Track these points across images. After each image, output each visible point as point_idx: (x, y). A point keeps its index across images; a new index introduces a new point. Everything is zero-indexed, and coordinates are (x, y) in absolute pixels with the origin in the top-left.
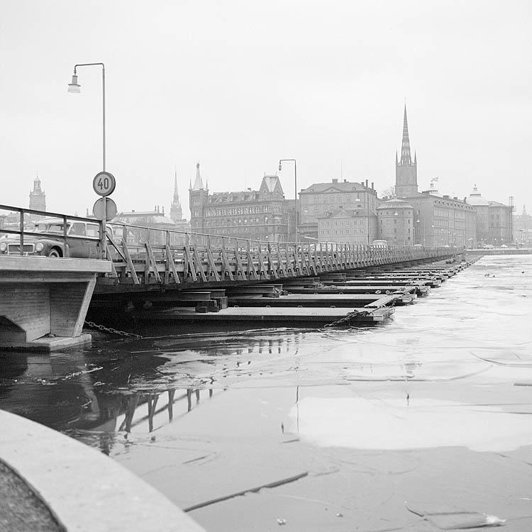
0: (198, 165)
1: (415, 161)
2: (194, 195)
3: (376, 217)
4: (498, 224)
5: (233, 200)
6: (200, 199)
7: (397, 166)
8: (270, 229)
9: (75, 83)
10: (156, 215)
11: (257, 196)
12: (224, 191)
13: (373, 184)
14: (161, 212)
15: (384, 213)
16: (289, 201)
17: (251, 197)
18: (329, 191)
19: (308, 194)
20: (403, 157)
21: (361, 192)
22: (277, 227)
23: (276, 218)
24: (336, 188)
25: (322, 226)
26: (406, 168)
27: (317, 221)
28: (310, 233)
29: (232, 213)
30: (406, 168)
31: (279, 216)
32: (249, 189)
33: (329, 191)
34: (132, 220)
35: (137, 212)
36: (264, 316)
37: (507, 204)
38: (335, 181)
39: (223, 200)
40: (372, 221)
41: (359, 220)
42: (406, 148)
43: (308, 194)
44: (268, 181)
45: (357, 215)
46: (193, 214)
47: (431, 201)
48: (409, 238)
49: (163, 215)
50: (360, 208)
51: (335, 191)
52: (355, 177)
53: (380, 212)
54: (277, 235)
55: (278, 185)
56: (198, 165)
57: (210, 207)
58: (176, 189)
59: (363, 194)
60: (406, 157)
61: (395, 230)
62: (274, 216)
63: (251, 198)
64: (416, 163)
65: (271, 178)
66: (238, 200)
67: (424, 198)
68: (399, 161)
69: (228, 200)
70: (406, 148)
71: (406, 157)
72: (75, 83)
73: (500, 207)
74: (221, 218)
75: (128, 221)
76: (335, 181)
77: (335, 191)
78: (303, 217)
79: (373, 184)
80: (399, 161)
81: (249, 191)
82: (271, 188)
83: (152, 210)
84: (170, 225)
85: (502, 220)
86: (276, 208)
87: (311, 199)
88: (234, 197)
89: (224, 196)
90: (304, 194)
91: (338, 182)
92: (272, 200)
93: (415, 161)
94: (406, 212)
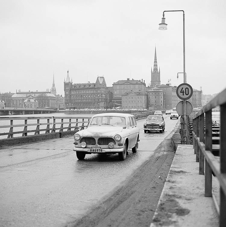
0: (68, 72)
1: (160, 71)
2: (66, 85)
3: (147, 95)
4: (195, 98)
5: (89, 87)
6: (68, 86)
7: (152, 73)
8: (100, 100)
9: (163, 23)
10: (47, 93)
11: (95, 85)
12: (79, 83)
13: (144, 81)
14: (49, 92)
15: (151, 93)
16: (108, 87)
17: (92, 86)
18: (126, 84)
19: (117, 85)
20: (154, 69)
21: (140, 84)
22: (103, 99)
23: (103, 95)
24: (128, 82)
25: (124, 99)
26: (156, 74)
27: (121, 97)
28: (118, 102)
29: (78, 93)
30: (156, 74)
31: (105, 94)
32: (89, 82)
33: (126, 84)
34: (37, 95)
35: (39, 91)
36: (32, 114)
37: (199, 90)
38: (128, 79)
39: (79, 87)
40: (146, 96)
41: (140, 97)
42: (156, 65)
43: (117, 85)
44: (99, 79)
45: (139, 94)
46: (65, 93)
47: (171, 88)
48: (161, 105)
49: (50, 93)
50: (140, 91)
51: (128, 83)
52: (137, 78)
53: (149, 93)
54: (103, 103)
55: (104, 81)
56: (68, 72)
57: (73, 90)
58: (54, 81)
59: (140, 85)
60: (156, 69)
61: (156, 101)
62: (102, 94)
63: (92, 86)
64: (160, 72)
65: (101, 77)
66: (86, 87)
67: (167, 87)
68: (153, 71)
69: (81, 87)
70: (156, 65)
71: (156, 69)
72: (163, 23)
73: (196, 91)
74: (78, 95)
75: (35, 95)
76: (128, 79)
77: (128, 83)
78: (114, 95)
79: (144, 81)
80: (153, 71)
81: (89, 83)
82: (101, 82)
83: (45, 91)
84: (53, 97)
85: (197, 97)
86: (103, 90)
87: (118, 87)
88: (89, 85)
89: (80, 85)
90: (115, 85)
91: (130, 80)
92: (101, 87)
93: (160, 71)
94: (160, 93)
